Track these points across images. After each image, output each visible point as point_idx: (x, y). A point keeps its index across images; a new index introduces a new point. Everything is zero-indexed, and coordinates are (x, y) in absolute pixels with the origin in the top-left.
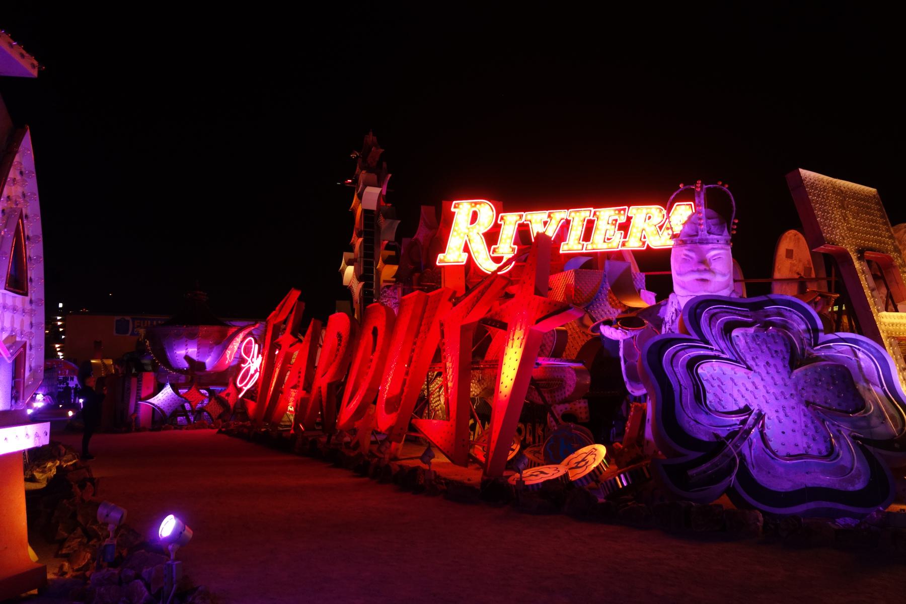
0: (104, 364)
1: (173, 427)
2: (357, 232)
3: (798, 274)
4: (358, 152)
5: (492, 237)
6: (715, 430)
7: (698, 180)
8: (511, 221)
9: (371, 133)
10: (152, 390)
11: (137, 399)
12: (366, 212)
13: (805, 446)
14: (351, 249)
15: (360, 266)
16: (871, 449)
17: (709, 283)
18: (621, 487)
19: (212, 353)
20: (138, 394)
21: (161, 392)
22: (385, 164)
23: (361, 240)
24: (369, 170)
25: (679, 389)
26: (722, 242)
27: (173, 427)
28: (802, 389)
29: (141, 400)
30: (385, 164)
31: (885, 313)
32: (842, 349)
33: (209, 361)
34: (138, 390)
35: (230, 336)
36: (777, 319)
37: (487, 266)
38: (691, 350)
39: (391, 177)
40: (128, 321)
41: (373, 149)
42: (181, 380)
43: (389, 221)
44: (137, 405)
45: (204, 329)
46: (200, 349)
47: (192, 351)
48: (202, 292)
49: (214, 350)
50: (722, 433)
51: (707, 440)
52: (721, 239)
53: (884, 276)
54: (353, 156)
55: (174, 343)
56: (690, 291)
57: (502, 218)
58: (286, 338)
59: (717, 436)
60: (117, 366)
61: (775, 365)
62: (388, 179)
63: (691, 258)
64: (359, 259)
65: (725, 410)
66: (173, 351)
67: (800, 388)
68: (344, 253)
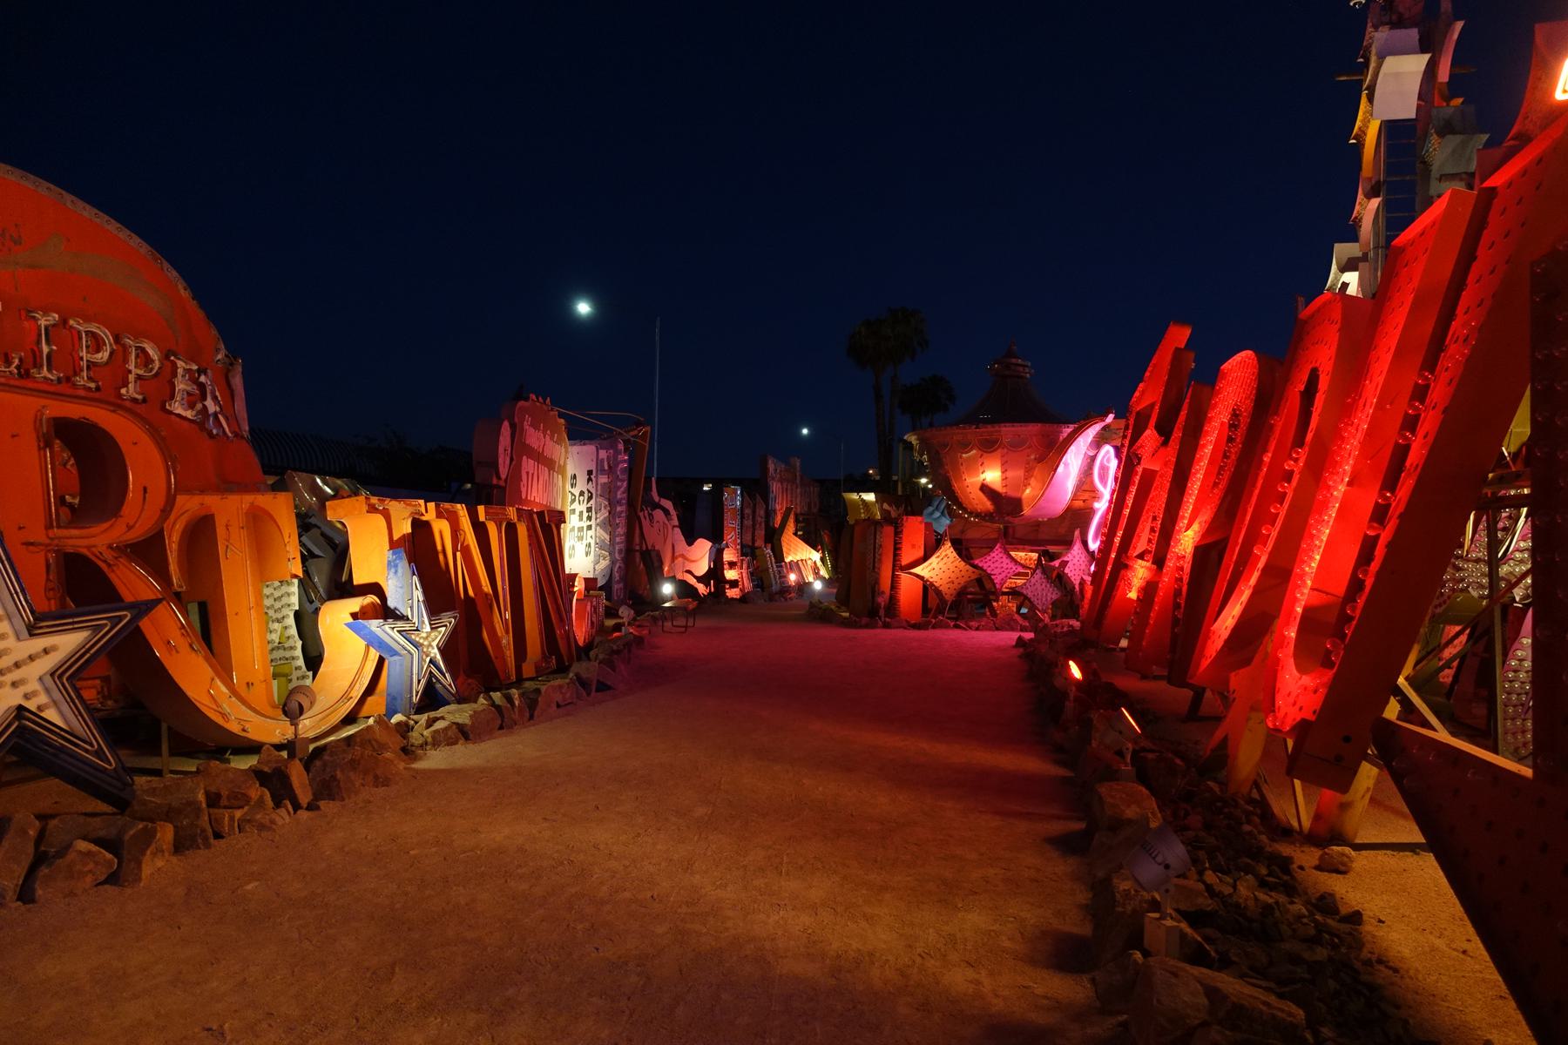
10: (921, 553)
11: (894, 566)
12: (1392, 129)
14: (1352, 235)
15: (1376, 270)
19: (1033, 479)
20: (896, 556)
23: (1375, 203)
35: (1065, 439)
43: (1453, 140)
45: (1007, 431)
46: (1007, 473)
47: (992, 476)
49: (1036, 471)
53: (936, 610)
58: (1150, 436)
60: (886, 506)
62: (1456, 36)
64: (1371, 254)
66: (961, 477)
68: (1336, 245)
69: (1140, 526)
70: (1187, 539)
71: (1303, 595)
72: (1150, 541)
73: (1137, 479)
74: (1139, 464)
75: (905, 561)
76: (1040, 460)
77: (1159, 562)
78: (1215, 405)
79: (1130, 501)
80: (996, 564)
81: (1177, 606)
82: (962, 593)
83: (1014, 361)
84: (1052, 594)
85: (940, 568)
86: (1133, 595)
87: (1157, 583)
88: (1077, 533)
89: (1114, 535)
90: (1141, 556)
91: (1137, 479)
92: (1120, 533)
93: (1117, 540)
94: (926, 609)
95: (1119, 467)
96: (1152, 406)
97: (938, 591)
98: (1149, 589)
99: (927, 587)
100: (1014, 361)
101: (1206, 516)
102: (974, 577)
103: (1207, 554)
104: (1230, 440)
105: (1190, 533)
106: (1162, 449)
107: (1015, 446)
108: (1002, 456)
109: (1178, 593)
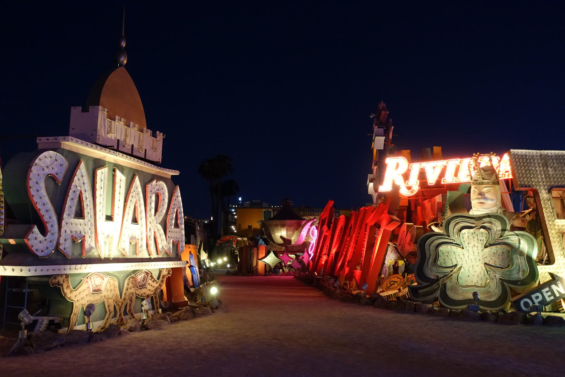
0: (243, 240)
1: (274, 274)
2: (375, 162)
3: (560, 195)
4: (374, 114)
5: (406, 176)
6: (438, 274)
7: (477, 152)
8: (416, 167)
9: (382, 102)
10: (264, 255)
11: (257, 259)
13: (476, 282)
14: (372, 173)
16: (505, 284)
17: (485, 204)
18: (407, 297)
20: (257, 256)
21: (268, 256)
22: (391, 120)
23: (376, 167)
24: (380, 125)
25: (429, 257)
26: (490, 183)
27: (274, 274)
28: (486, 257)
29: (259, 260)
30: (391, 120)
31: (557, 220)
32: (514, 239)
33: (294, 239)
34: (257, 254)
36: (487, 225)
37: (404, 192)
38: (440, 239)
39: (394, 128)
40: (271, 212)
41: (382, 112)
42: (283, 249)
44: (257, 262)
45: (288, 222)
48: (289, 201)
49: (295, 233)
50: (440, 275)
51: (433, 278)
52: (490, 182)
54: (372, 117)
55: (275, 229)
56: (477, 209)
57: (411, 166)
59: (437, 276)
60: (249, 242)
61: (477, 247)
63: (476, 192)
65: (446, 266)
67: (485, 257)
68: (369, 175)
69: (324, 248)
70: (334, 251)
71: (348, 258)
72: (326, 251)
73: (323, 237)
74: (323, 233)
75: (260, 258)
76: (297, 229)
77: (328, 255)
78: (338, 225)
79: (321, 242)
80: (285, 258)
81: (332, 263)
82: (276, 267)
83: (288, 201)
84: (300, 266)
85: (271, 259)
86: (323, 263)
87: (328, 260)
88: (306, 249)
89: (318, 250)
90: (325, 254)
91: (323, 237)
92: (319, 249)
93: (319, 251)
94: (266, 271)
95: (318, 232)
96: (326, 218)
97: (269, 266)
98: (326, 261)
99: (266, 265)
100: (288, 201)
101: (337, 246)
102: (279, 262)
103: (337, 253)
104: (341, 232)
105: (334, 250)
106: (328, 231)
107: (290, 226)
108: (287, 228)
109: (332, 261)
